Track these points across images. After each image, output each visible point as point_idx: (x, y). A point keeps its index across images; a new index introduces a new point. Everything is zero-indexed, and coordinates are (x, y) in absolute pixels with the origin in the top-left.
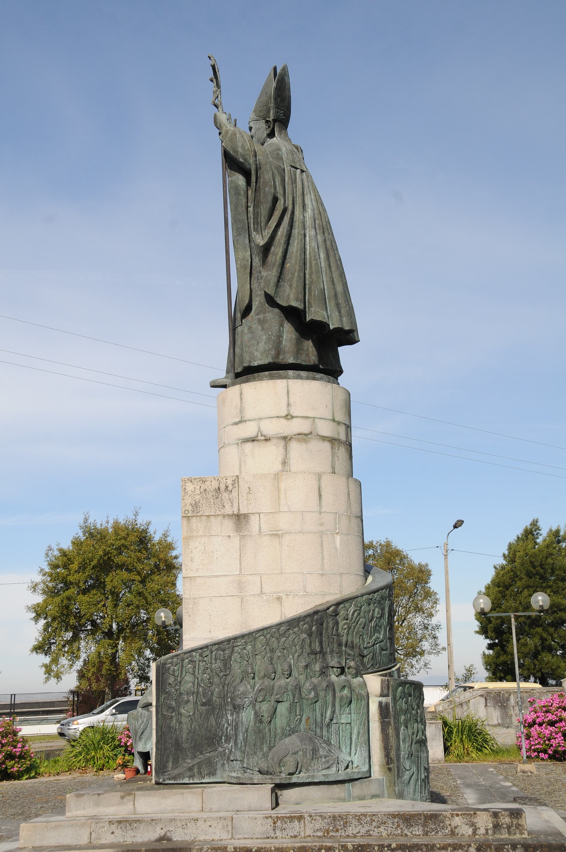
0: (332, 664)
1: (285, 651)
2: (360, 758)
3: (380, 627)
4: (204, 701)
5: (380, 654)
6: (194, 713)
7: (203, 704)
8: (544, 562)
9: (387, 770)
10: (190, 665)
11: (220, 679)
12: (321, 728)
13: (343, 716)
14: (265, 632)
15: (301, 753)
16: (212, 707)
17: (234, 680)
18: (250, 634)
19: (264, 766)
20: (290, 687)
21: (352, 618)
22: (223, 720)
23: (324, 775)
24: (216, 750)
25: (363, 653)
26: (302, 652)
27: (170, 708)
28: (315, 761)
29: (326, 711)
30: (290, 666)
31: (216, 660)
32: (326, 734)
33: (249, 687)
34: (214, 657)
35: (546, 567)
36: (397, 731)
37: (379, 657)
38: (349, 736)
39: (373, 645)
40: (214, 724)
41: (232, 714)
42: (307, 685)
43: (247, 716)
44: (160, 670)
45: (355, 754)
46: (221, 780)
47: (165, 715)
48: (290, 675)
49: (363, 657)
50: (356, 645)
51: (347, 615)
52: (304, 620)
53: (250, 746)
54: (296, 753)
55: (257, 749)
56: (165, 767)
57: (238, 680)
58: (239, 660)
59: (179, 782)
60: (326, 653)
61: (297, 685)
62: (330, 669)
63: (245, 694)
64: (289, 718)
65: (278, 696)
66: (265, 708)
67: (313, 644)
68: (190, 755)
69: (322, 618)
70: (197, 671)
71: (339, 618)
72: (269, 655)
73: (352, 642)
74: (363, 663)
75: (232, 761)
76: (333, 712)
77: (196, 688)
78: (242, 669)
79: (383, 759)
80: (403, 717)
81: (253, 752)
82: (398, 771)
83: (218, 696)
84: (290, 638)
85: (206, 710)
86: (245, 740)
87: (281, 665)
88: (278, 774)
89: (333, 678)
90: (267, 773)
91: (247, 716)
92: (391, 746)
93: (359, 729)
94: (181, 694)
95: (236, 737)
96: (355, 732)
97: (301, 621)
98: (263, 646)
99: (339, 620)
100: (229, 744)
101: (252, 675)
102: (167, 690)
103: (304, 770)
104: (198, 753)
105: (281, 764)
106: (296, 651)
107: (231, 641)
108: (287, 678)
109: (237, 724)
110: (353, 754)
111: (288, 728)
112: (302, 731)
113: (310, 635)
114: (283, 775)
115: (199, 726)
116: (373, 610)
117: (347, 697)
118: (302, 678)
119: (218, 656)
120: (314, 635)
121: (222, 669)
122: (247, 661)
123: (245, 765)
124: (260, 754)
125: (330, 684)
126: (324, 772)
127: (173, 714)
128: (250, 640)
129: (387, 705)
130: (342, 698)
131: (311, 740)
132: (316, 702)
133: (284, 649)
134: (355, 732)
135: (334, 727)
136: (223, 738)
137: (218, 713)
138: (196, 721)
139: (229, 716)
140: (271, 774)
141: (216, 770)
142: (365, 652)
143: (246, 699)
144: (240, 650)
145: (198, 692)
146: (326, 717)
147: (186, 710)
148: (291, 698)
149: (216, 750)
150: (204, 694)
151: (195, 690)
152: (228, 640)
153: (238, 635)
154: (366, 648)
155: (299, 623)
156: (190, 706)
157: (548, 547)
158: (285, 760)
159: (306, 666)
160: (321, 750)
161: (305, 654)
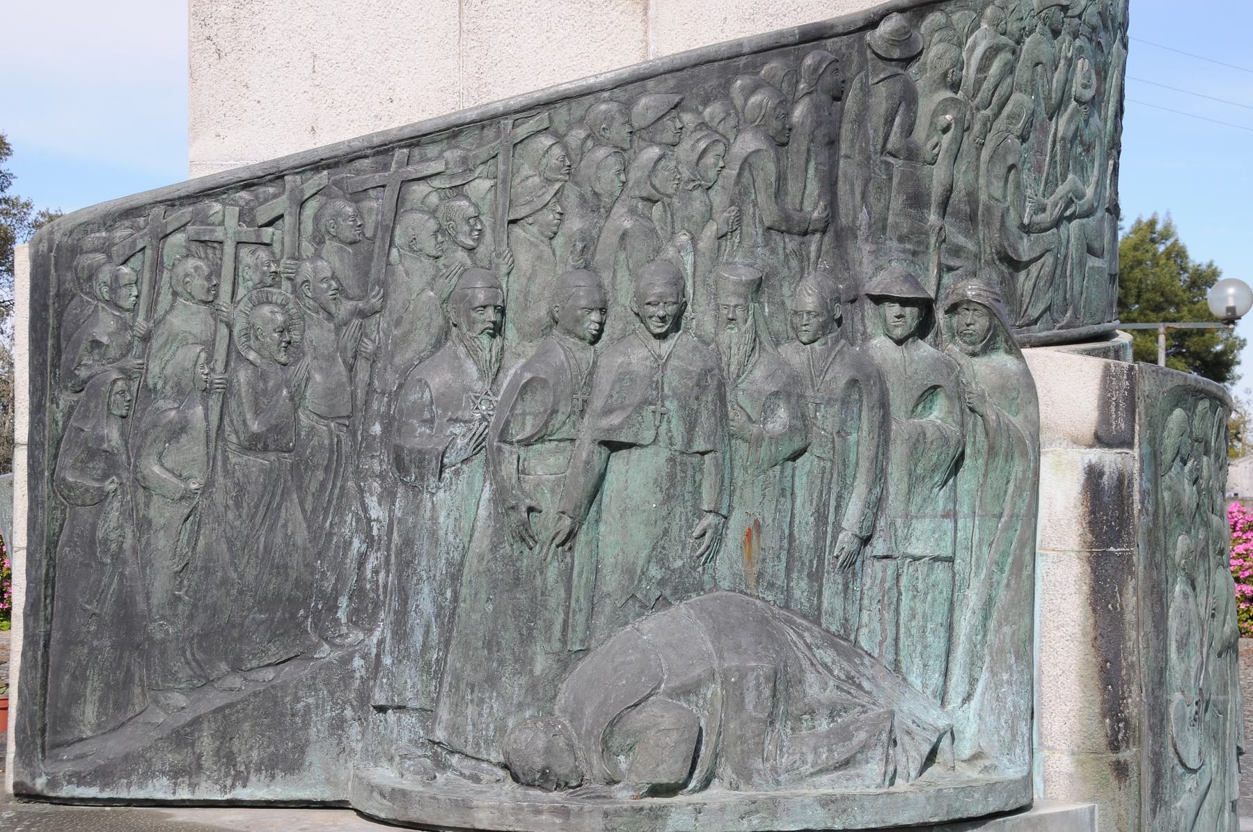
0: (875, 286)
1: (657, 210)
2: (990, 720)
3: (1088, 148)
4: (255, 427)
5: (1082, 264)
6: (209, 484)
7: (254, 444)
8: (1125, 276)
9: (1108, 771)
10: (191, 263)
11: (338, 329)
12: (816, 577)
13: (920, 526)
14: (562, 113)
15: (713, 690)
16: (289, 458)
17: (405, 337)
18: (486, 122)
19: (530, 741)
20: (672, 380)
21: (978, 83)
22: (342, 522)
23: (826, 802)
24: (305, 656)
25: (1016, 250)
26: (739, 219)
27: (92, 454)
28: (783, 729)
29: (840, 497)
30: (678, 282)
31: (318, 240)
32: (838, 602)
33: (471, 368)
34: (308, 226)
35: (1131, 284)
36: (1158, 596)
37: (1077, 279)
38: (940, 618)
39: (1057, 224)
40: (302, 536)
41: (388, 496)
42: (759, 373)
43: (459, 507)
44: (46, 275)
45: (968, 698)
46: (327, 795)
47: (70, 488)
48: (676, 323)
49: (1016, 265)
50: (988, 209)
51: (959, 64)
52: (753, 68)
53: (467, 644)
54: (688, 691)
55: (502, 662)
56: (65, 720)
57: (422, 340)
58: (430, 246)
59: (124, 794)
60: (853, 231)
61: (707, 371)
62: (869, 307)
63: (450, 405)
64: (661, 525)
65: (615, 419)
66: (547, 472)
67: (792, 187)
68: (185, 673)
69: (838, 63)
70: (226, 288)
71: (921, 77)
72: (575, 224)
73: (972, 197)
74: (1010, 296)
75: (381, 709)
76: (877, 506)
77: (220, 366)
78: (446, 287)
79: (1095, 724)
80: (1182, 543)
81: (481, 675)
82: (1158, 776)
83: (322, 410)
84: (686, 151)
85: (267, 472)
86: (448, 616)
87: (635, 275)
88: (598, 787)
89: (881, 347)
90: (545, 779)
91: (459, 507)
92: (1132, 666)
93: (991, 584)
94: (149, 392)
95: (404, 601)
96: (972, 598)
97: (737, 73)
98: (549, 181)
99: (921, 85)
100: (370, 631)
101: (491, 314)
102: (83, 373)
103: (726, 771)
104: (224, 667)
105: (616, 742)
106: (709, 216)
107: (390, 154)
108: (662, 337)
109: (408, 543)
110: (955, 698)
111: (655, 572)
112: (725, 584)
113: (780, 141)
114: (623, 796)
115: (230, 543)
116: (1070, 63)
117: (945, 440)
118: (734, 339)
119: (326, 220)
120: (799, 144)
121: (350, 283)
122: (471, 250)
123: (440, 735)
124: (514, 686)
125: (869, 377)
126: (827, 785)
127: (109, 486)
128: (484, 152)
129: (1122, 482)
130: (917, 443)
131: (766, 630)
132: (795, 457)
133: (651, 201)
134: (972, 598)
135: (873, 574)
136: (343, 602)
137: (323, 485)
138: (218, 520)
139: (372, 502)
140: (562, 785)
141: (301, 749)
142: (1025, 248)
143: (458, 429)
144: (434, 199)
145: (228, 390)
146: (838, 528)
147: (172, 469)
148: (677, 428)
149: (305, 656)
150: (256, 396)
151: (216, 377)
152: (382, 150)
153: (428, 127)
154: (1027, 229)
155: (727, 85)
156: (192, 449)
157: (1136, 248)
158: (638, 719)
159: (757, 287)
160: (811, 677)
161: (753, 231)
